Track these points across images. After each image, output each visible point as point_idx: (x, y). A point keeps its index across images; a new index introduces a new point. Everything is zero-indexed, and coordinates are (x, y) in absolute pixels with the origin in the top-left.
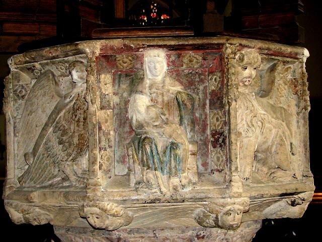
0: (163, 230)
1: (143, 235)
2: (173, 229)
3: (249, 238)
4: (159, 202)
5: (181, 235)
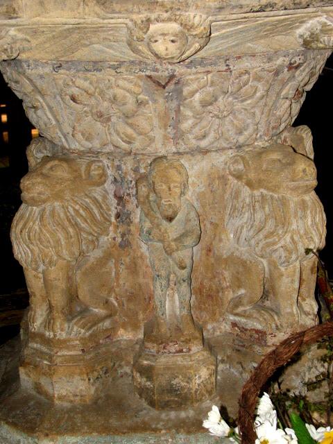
0: (239, 57)
1: (210, 68)
2: (254, 56)
3: (9, 74)
4: (271, 9)
5: (267, 66)
